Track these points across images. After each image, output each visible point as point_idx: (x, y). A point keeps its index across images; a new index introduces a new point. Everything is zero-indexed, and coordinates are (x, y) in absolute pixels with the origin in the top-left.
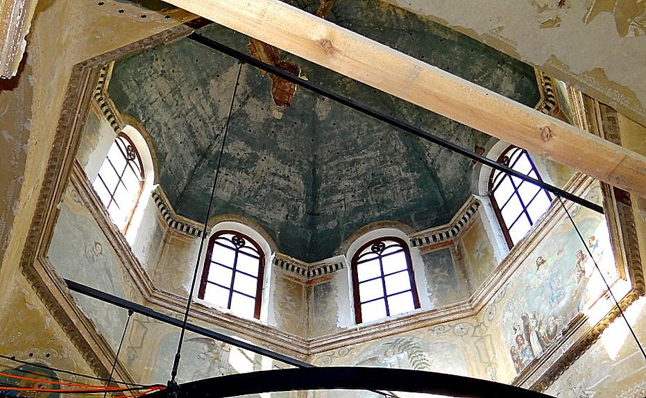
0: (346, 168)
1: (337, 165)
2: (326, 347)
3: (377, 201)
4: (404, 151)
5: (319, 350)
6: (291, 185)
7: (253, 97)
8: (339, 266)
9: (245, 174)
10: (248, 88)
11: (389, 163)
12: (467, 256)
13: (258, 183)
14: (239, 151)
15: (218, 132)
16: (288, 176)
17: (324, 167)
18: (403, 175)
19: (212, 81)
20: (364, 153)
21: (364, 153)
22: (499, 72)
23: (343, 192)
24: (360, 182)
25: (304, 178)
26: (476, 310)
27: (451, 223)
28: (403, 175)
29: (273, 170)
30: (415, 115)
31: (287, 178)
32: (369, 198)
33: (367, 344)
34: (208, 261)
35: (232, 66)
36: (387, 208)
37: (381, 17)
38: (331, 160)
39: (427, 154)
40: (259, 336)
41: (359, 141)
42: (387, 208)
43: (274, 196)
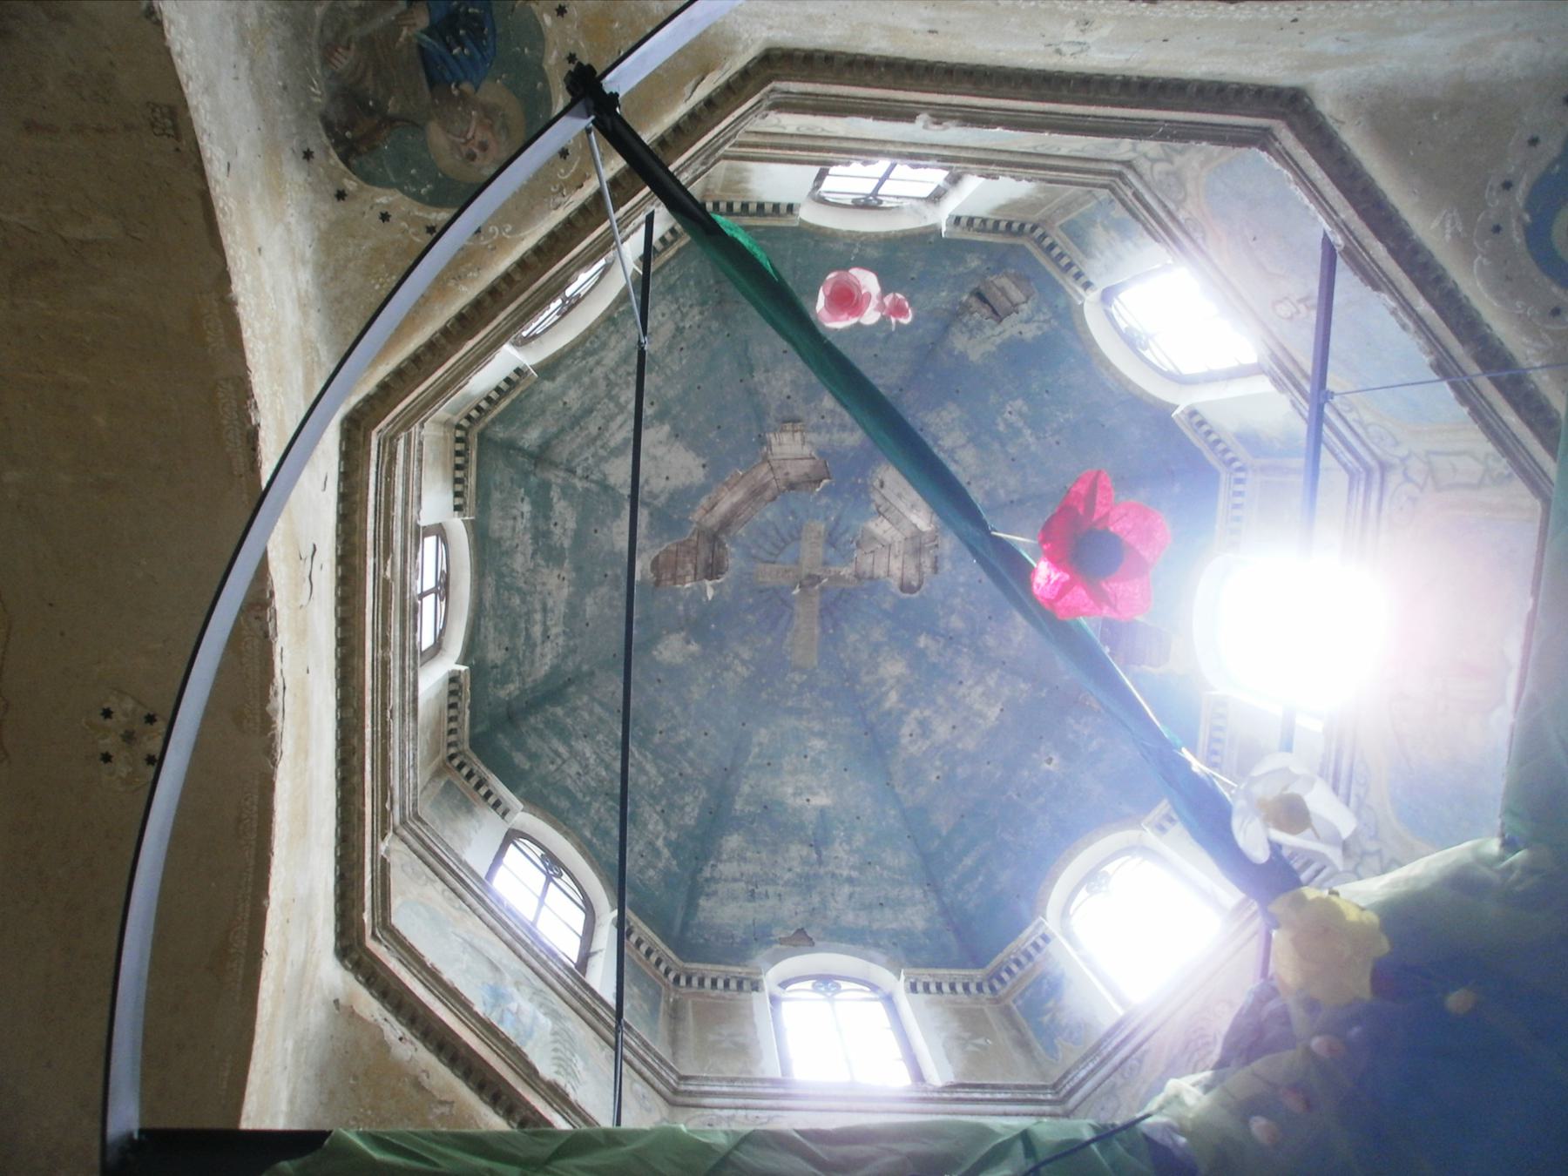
0: (607, 737)
1: (600, 719)
2: (431, 860)
3: (600, 820)
4: (689, 823)
5: (417, 846)
6: (538, 650)
7: (651, 514)
8: (501, 809)
10: (663, 499)
11: (659, 808)
13: (525, 582)
14: (560, 523)
15: (579, 471)
17: (585, 698)
18: (660, 843)
19: (667, 428)
20: (645, 757)
21: (645, 757)
22: (918, 893)
24: (604, 773)
25: (555, 669)
26: (680, 1099)
27: (687, 965)
28: (660, 843)
29: (550, 603)
31: (546, 636)
32: (596, 805)
35: (698, 455)
36: (604, 845)
37: (868, 673)
38: (601, 704)
39: (712, 862)
42: (604, 845)
43: (515, 625)
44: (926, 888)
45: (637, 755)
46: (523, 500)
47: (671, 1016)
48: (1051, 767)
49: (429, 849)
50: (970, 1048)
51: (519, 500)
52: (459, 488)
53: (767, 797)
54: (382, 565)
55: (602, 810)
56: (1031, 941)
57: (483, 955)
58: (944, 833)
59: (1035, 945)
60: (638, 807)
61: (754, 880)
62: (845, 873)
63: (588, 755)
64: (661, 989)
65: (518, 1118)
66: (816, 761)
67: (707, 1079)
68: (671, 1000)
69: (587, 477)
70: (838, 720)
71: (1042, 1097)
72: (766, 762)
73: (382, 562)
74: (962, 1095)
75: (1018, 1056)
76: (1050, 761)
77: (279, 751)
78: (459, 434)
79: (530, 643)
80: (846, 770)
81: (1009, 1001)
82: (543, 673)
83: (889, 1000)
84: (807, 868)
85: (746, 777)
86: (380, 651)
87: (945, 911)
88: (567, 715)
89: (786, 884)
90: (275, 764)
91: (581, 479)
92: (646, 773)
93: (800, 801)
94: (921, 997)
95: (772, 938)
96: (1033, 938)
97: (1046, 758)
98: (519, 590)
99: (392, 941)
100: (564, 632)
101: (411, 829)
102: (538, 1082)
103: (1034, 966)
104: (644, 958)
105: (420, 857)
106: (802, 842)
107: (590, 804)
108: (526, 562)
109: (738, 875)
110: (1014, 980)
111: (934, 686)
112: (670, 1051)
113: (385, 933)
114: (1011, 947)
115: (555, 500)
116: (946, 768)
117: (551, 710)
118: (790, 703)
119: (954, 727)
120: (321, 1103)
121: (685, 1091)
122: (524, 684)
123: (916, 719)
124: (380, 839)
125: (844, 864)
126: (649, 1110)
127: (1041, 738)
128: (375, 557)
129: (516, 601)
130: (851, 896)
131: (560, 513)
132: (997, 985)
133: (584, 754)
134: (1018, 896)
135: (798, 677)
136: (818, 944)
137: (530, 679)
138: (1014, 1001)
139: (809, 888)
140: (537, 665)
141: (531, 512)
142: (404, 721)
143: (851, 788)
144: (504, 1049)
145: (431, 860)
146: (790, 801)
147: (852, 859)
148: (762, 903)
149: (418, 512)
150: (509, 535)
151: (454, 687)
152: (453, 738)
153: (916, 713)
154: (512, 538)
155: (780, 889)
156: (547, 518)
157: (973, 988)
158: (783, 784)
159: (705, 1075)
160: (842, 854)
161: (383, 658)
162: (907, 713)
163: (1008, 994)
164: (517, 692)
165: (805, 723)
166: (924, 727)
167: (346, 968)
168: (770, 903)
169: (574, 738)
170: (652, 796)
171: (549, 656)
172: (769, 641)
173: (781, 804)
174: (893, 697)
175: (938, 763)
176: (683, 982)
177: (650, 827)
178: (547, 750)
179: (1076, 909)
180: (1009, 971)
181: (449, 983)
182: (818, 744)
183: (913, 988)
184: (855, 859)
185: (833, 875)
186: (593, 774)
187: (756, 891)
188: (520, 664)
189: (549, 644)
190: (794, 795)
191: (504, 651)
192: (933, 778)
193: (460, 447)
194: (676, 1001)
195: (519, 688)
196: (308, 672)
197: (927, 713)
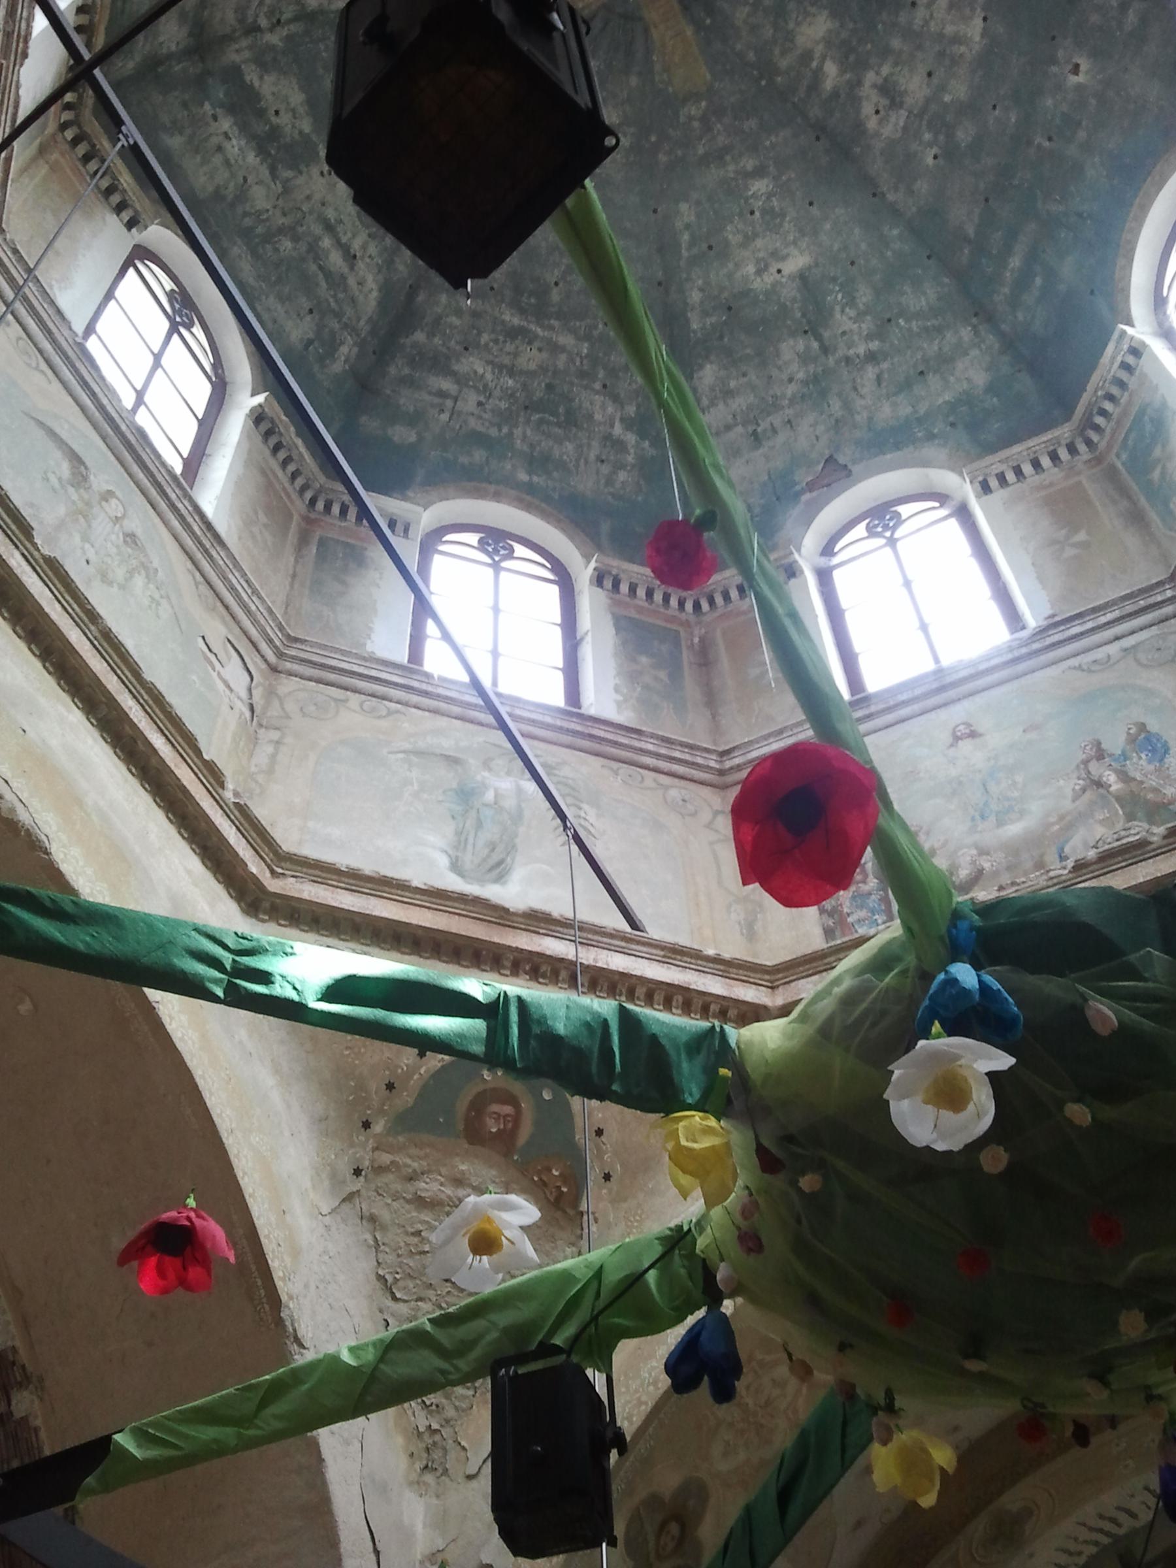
1: (475, 314)
2: (332, 677)
3: (532, 446)
6: (352, 281)
9: (267, 172)
11: (597, 386)
12: (724, 662)
13: (284, 214)
14: (282, 108)
15: (263, 22)
16: (355, 257)
18: (618, 430)
21: (551, 328)
22: (966, 333)
23: (462, 381)
24: (510, 382)
28: (618, 430)
29: (331, 214)
30: (714, 319)
31: (351, 258)
32: (518, 432)
33: (443, 722)
34: (109, 295)
37: (783, 53)
40: (189, 542)
41: (555, 296)
44: (974, 320)
45: (539, 331)
46: (215, 118)
47: (700, 665)
48: (1080, 78)
49: (323, 666)
50: (1070, 552)
51: (210, 120)
52: (116, 199)
53: (726, 294)
54: (32, 549)
55: (529, 432)
56: (1116, 365)
57: (436, 755)
58: (971, 231)
59: (1125, 366)
60: (572, 400)
61: (752, 416)
62: (861, 350)
63: (480, 371)
64: (677, 632)
65: (508, 964)
66: (768, 212)
67: (750, 743)
68: (696, 640)
69: (279, 21)
70: (773, 139)
71: (1159, 598)
72: (704, 246)
73: (29, 545)
74: (1056, 638)
75: (1132, 540)
76: (1076, 69)
77: (44, 838)
78: (69, 134)
79: (337, 282)
80: (811, 204)
81: (1112, 457)
82: (373, 303)
83: (963, 513)
84: (811, 368)
85: (688, 279)
86: (93, 628)
87: (1009, 344)
88: (430, 335)
89: (792, 401)
90: (48, 853)
91: (271, 29)
92: (563, 349)
93: (769, 278)
94: (999, 495)
95: (798, 488)
96: (1119, 359)
97: (1070, 67)
98: (281, 231)
99: (295, 867)
100: (370, 235)
101: (293, 657)
102: (515, 918)
103: (1131, 395)
104: (646, 604)
105: (319, 681)
106: (793, 334)
107: (510, 434)
108: (269, 188)
109: (730, 418)
110: (1112, 424)
111: (880, 26)
112: (708, 713)
113: (283, 864)
114: (1095, 378)
115: (256, 84)
116: (941, 138)
117: (408, 341)
118: (701, 151)
119: (930, 74)
120: (308, 1052)
121: (732, 768)
122: (358, 335)
123: (874, 86)
124: (220, 791)
125: (856, 338)
126: (694, 814)
127: (1053, 38)
128: (17, 547)
129: (287, 245)
130: (879, 379)
131: (273, 94)
132: (1095, 437)
133: (475, 372)
134: (1092, 292)
135: (694, 110)
136: (856, 469)
137: (362, 323)
138: (1118, 456)
139: (823, 394)
140: (361, 298)
141: (235, 123)
142: (211, 557)
143: (828, 226)
144: (463, 906)
145: (332, 677)
146: (757, 284)
147: (864, 326)
148: (771, 443)
149: (70, 329)
150: (227, 175)
151: (264, 426)
152: (300, 481)
153: (870, 77)
154: (233, 175)
155: (789, 412)
156: (261, 113)
157: (1063, 454)
158: (737, 266)
159: (746, 740)
160: (848, 325)
161: (100, 631)
162: (860, 83)
163: (1109, 446)
164: (356, 350)
165: (731, 168)
166: (891, 93)
167: (263, 921)
168: (781, 439)
169: (453, 361)
170: (582, 374)
171: (370, 278)
172: (634, 81)
173: (746, 293)
174: (831, 69)
175: (927, 136)
176: (705, 606)
177: (598, 417)
178: (427, 397)
179: (1170, 287)
180: (1103, 413)
181: (374, 875)
182: (760, 186)
183: (986, 488)
184: (867, 325)
185: (848, 360)
186: (497, 393)
187: (759, 430)
188: (338, 315)
189: (360, 265)
190: (759, 272)
191: (308, 318)
192: (930, 161)
193: (82, 149)
194: (702, 640)
195: (355, 344)
196: (24, 731)
197: (885, 70)
